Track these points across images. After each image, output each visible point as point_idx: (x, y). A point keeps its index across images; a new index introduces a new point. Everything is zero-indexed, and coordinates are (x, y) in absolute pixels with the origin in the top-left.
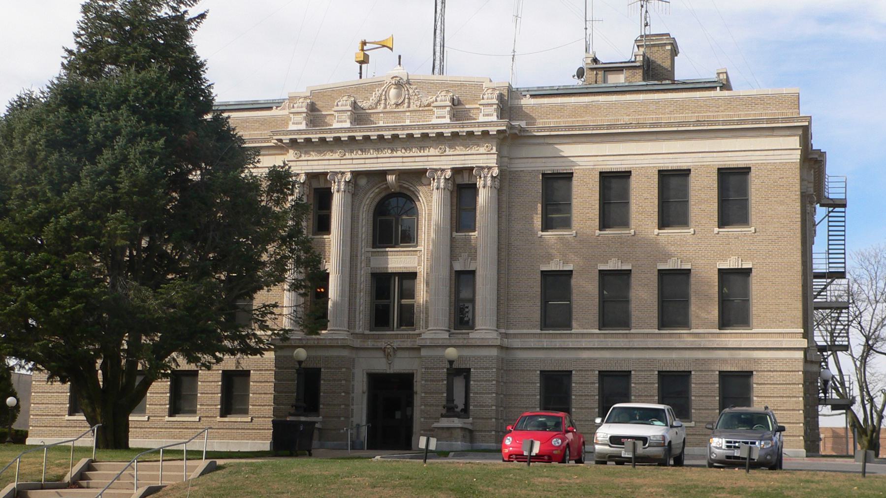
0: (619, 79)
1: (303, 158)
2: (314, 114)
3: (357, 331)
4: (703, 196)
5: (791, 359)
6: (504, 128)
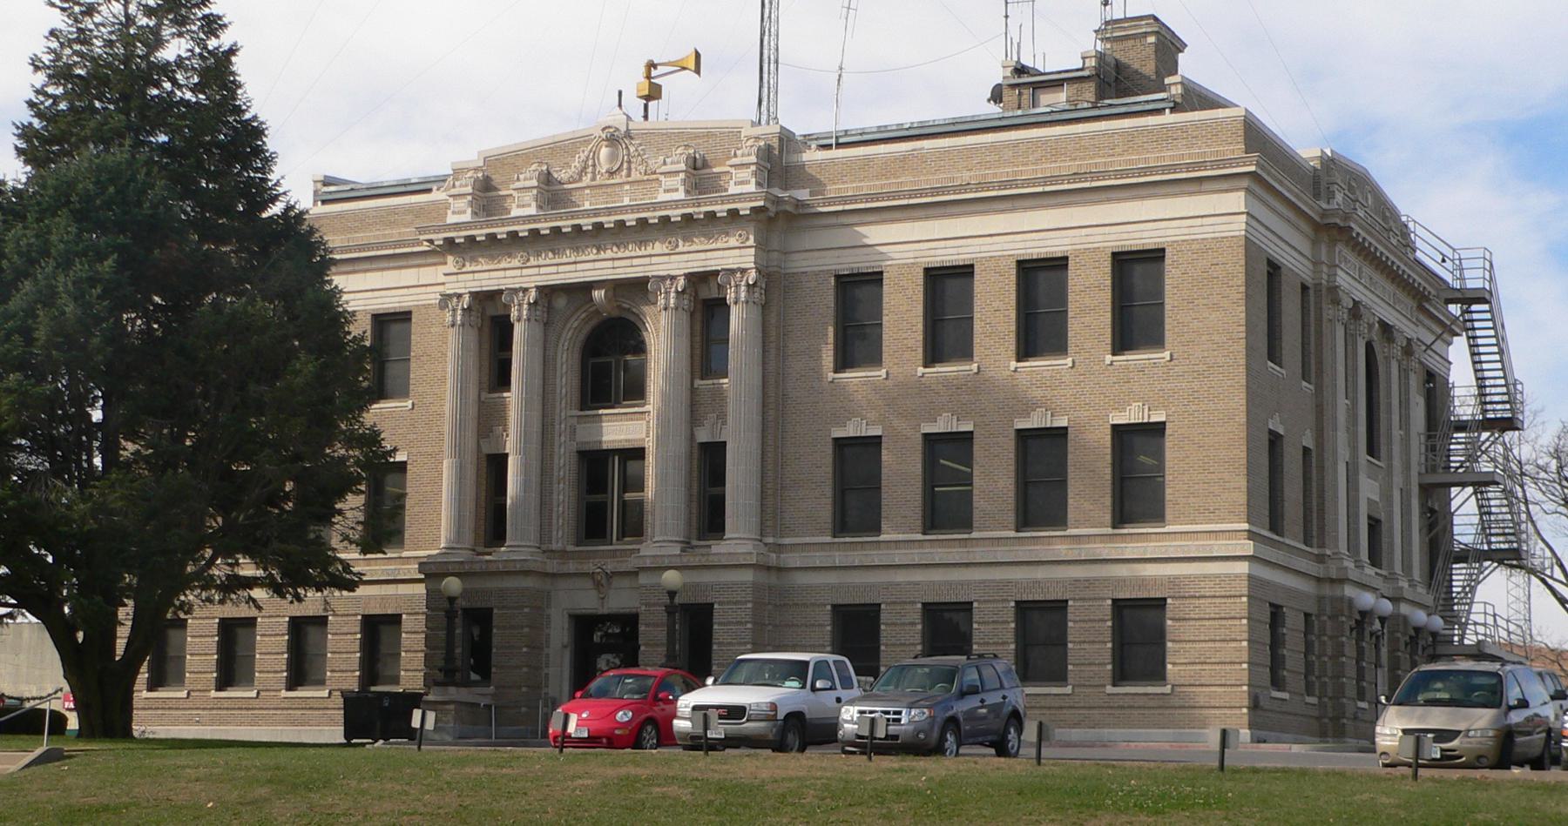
0: (1060, 98)
1: (468, 268)
2: (486, 194)
3: (554, 546)
4: (1087, 301)
5: (1228, 575)
6: (761, 203)
